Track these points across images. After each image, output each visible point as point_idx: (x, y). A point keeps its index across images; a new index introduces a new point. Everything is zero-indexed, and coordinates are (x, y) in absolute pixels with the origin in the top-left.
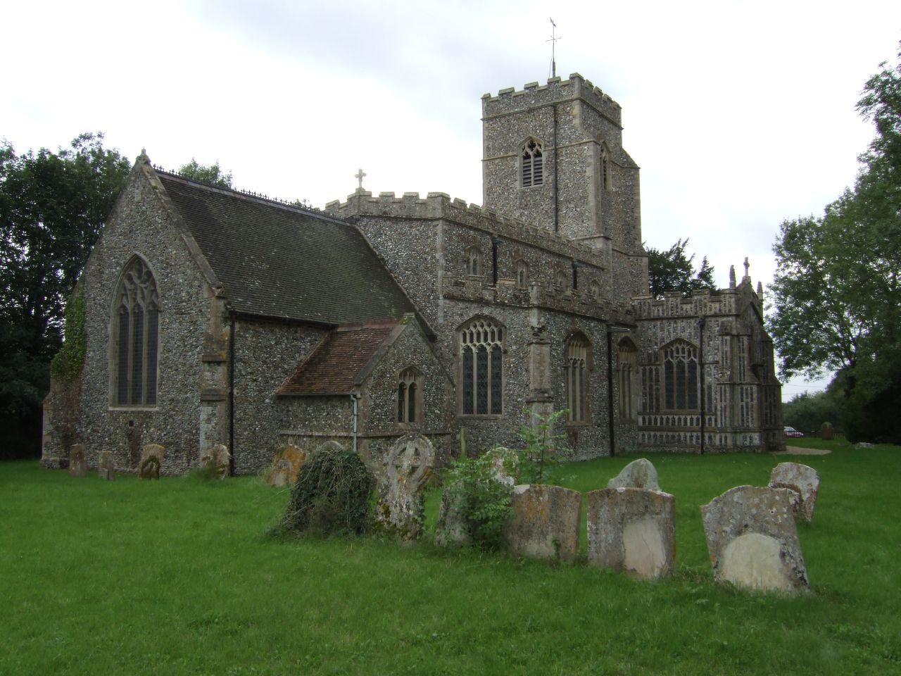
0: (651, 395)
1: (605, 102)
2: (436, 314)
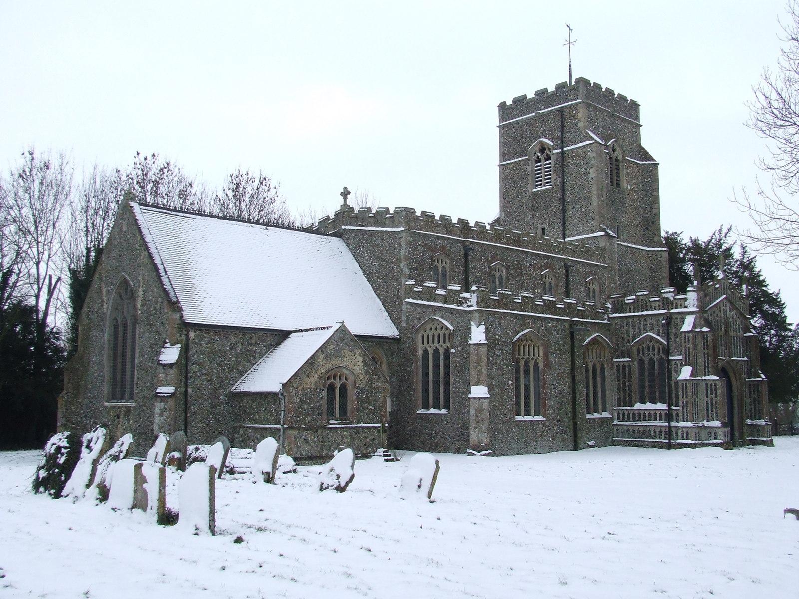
0: (624, 391)
1: (617, 102)
2: (400, 318)
